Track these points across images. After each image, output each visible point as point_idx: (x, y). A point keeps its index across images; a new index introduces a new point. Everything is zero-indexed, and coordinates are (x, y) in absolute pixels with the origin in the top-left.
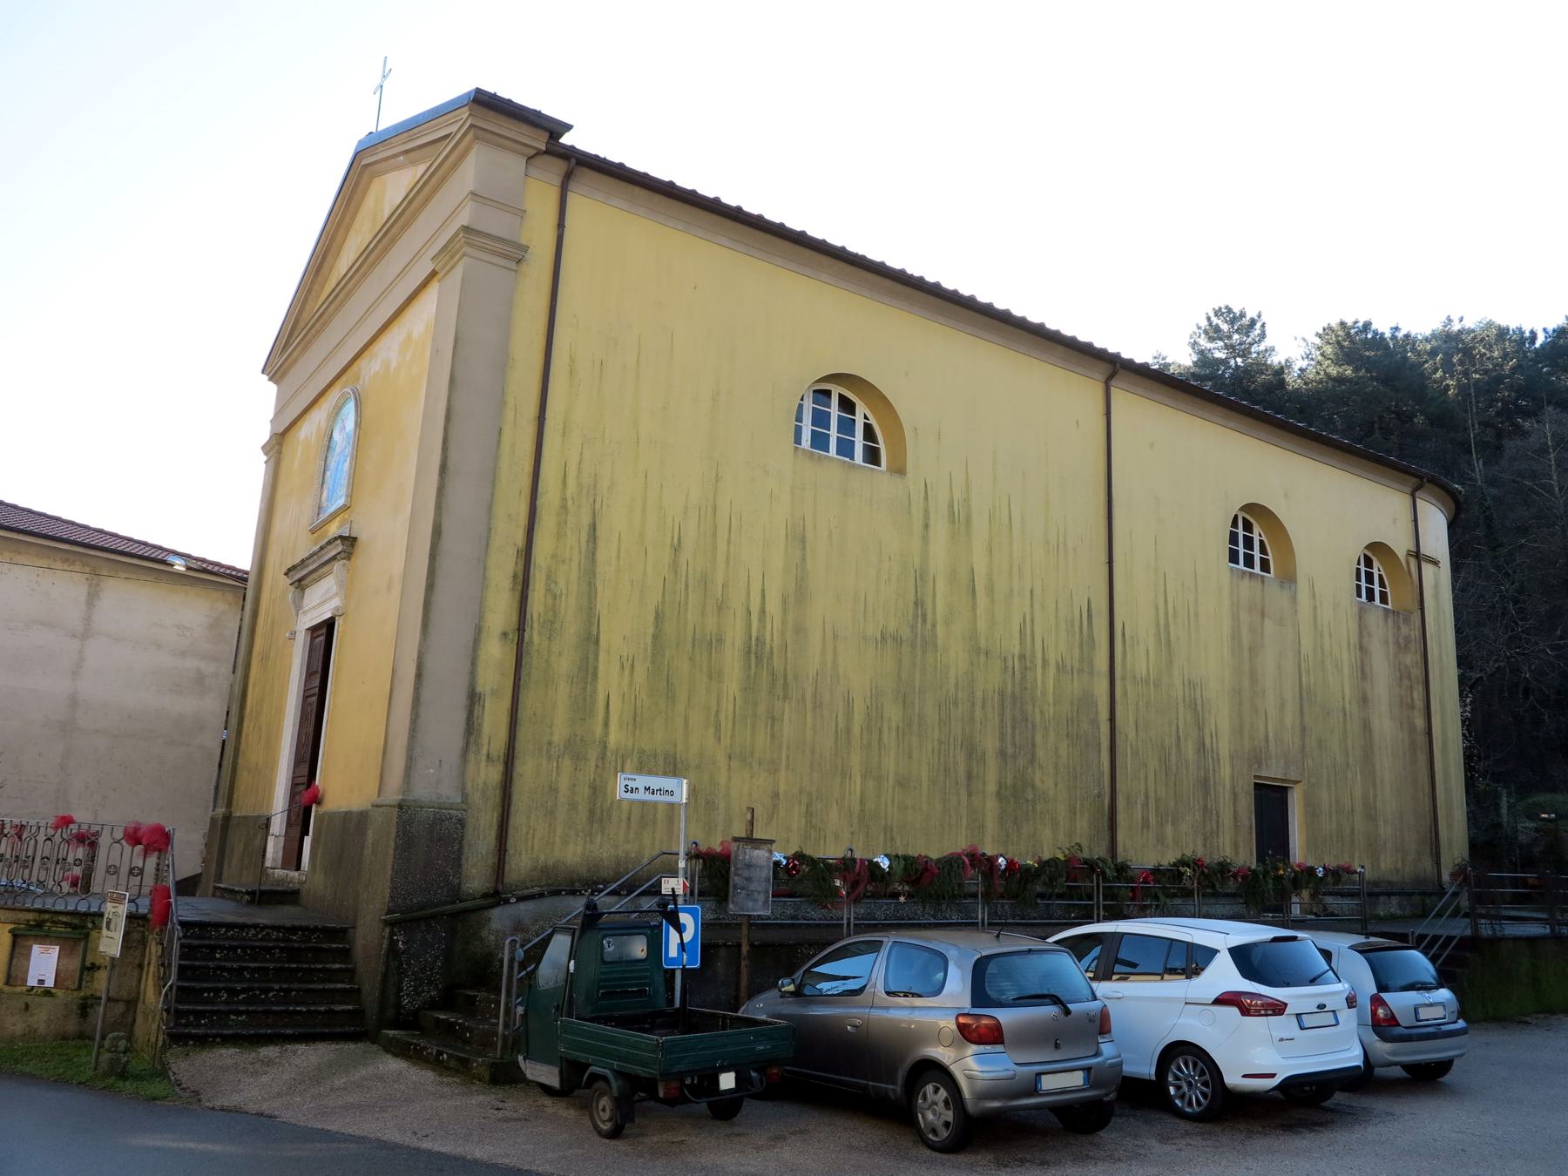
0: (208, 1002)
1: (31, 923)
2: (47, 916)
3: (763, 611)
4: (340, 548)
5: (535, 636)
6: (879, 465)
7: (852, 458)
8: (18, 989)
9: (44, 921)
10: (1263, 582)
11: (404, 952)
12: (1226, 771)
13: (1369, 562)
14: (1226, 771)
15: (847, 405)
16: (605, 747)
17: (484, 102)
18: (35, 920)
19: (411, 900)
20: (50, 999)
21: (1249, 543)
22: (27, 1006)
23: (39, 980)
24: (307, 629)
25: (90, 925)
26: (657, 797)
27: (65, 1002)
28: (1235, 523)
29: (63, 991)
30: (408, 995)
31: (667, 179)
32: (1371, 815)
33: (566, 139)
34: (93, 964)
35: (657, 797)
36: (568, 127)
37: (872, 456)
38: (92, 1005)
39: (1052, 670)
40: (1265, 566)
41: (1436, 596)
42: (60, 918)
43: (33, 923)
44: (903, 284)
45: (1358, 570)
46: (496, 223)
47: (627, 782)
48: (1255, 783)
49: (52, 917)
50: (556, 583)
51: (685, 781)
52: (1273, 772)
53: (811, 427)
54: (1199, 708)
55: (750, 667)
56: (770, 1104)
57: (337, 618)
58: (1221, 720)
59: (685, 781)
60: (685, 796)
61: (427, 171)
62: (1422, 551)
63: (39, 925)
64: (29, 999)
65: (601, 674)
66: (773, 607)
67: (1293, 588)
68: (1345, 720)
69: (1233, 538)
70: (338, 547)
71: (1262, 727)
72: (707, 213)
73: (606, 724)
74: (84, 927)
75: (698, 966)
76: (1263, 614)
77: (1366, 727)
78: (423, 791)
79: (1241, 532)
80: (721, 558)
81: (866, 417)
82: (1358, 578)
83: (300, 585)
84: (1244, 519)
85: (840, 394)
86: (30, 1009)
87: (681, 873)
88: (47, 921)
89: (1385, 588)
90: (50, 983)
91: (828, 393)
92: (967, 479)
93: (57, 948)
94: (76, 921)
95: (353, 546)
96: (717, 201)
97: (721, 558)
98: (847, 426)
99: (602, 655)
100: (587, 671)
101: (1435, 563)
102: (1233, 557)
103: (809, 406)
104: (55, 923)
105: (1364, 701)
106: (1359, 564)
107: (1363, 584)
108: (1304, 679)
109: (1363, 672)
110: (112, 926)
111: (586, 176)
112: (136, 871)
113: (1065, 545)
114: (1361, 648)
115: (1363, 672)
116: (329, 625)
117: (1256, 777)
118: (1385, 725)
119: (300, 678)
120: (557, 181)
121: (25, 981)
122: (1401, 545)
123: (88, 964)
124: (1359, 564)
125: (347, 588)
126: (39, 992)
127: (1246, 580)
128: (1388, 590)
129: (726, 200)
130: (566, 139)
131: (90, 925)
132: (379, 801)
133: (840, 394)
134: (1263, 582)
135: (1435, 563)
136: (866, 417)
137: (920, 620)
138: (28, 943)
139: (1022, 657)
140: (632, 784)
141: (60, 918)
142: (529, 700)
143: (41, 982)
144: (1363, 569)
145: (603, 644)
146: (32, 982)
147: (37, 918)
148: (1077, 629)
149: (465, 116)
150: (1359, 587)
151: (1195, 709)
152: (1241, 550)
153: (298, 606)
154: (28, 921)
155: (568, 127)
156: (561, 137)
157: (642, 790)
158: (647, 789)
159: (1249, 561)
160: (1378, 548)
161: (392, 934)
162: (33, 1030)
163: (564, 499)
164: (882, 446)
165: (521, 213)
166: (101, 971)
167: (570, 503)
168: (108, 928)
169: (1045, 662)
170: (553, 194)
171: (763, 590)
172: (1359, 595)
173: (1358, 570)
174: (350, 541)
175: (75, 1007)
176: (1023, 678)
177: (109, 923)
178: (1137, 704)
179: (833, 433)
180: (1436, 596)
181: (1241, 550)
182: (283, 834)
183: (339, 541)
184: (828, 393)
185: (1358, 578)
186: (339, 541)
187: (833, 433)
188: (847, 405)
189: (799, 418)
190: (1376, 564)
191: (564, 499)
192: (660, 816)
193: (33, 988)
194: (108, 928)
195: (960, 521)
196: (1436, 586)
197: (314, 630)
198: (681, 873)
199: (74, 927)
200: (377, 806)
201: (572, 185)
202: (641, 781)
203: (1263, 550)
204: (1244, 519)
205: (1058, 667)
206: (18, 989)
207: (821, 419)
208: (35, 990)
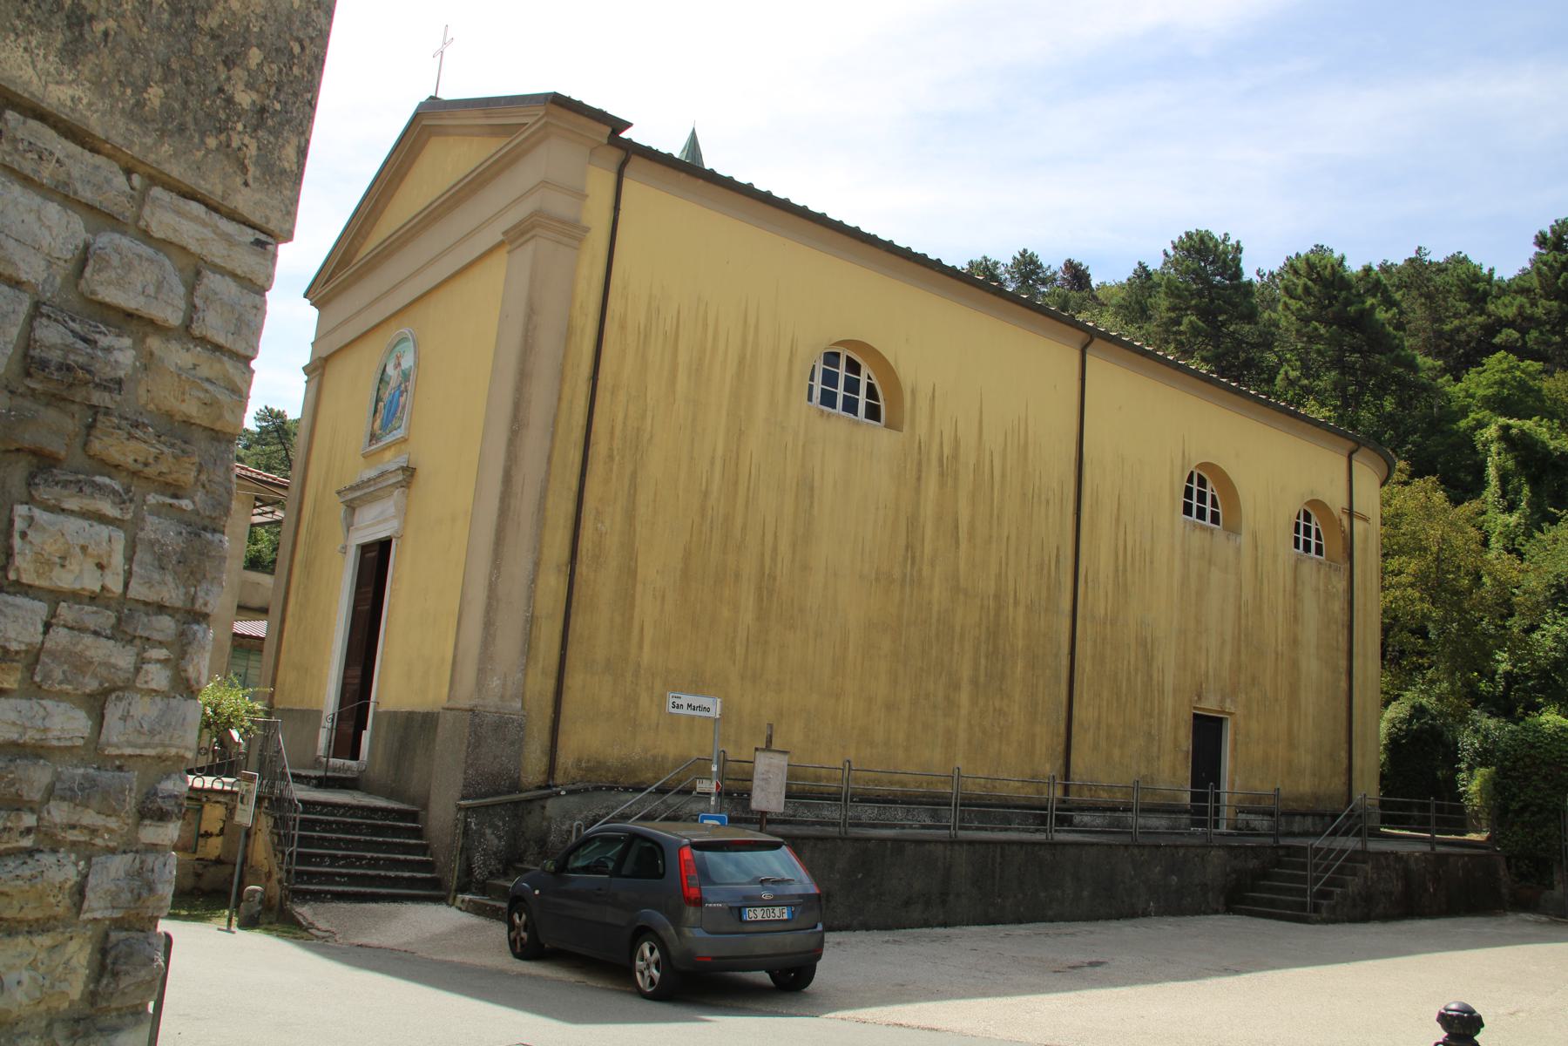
0: (315, 865)
3: (775, 549)
4: (400, 478)
5: (583, 569)
6: (879, 420)
7: (856, 414)
10: (1212, 533)
11: (476, 832)
12: (1169, 702)
13: (1307, 517)
14: (1169, 702)
15: (853, 366)
16: (639, 666)
17: (559, 102)
19: (480, 789)
21: (1307, 531)
24: (358, 545)
25: (204, 799)
26: (697, 713)
28: (1190, 480)
30: (479, 868)
31: (801, 205)
32: (1292, 745)
33: (625, 135)
34: (206, 832)
35: (697, 713)
36: (628, 125)
37: (873, 413)
39: (1021, 610)
40: (1319, 551)
41: (1365, 550)
45: (1297, 525)
46: (559, 205)
47: (674, 700)
48: (1194, 714)
50: (602, 522)
51: (719, 700)
52: (1210, 705)
53: (821, 386)
54: (1149, 646)
55: (762, 600)
56: (533, 963)
57: (394, 540)
58: (1167, 658)
59: (719, 700)
60: (718, 712)
61: (497, 152)
62: (1355, 509)
65: (638, 602)
66: (784, 547)
67: (1238, 540)
68: (1277, 659)
69: (1188, 493)
71: (1203, 665)
72: (965, 286)
73: (641, 647)
74: (199, 800)
76: (1210, 562)
77: (1295, 665)
78: (491, 701)
79: (1195, 487)
80: (741, 501)
81: (869, 378)
82: (1297, 531)
83: (351, 507)
84: (1199, 475)
85: (848, 357)
87: (714, 775)
89: (1217, 508)
91: (837, 355)
92: (956, 436)
95: (412, 475)
96: (805, 208)
97: (741, 501)
98: (852, 386)
99: (639, 587)
100: (626, 600)
101: (1365, 519)
102: (1187, 510)
103: (820, 367)
105: (1295, 642)
106: (1298, 518)
107: (1301, 537)
108: (1243, 622)
109: (1295, 617)
110: (245, 801)
111: (636, 162)
112: (203, 751)
113: (1040, 497)
114: (1295, 595)
115: (1295, 617)
116: (384, 546)
117: (1195, 708)
118: (1311, 666)
120: (615, 168)
122: (1337, 501)
123: (202, 832)
124: (1298, 518)
125: (404, 513)
127: (1197, 532)
128: (1220, 511)
129: (719, 171)
130: (625, 135)
131: (204, 799)
132: (451, 704)
133: (848, 357)
134: (1212, 533)
135: (1365, 519)
136: (869, 378)
137: (909, 562)
139: (997, 597)
140: (678, 702)
142: (577, 622)
144: (1302, 522)
145: (639, 577)
148: (1045, 572)
149: (541, 113)
150: (1297, 540)
151: (1146, 646)
152: (1195, 503)
153: (349, 526)
155: (628, 125)
156: (622, 131)
157: (685, 706)
158: (689, 706)
159: (1307, 548)
160: (1316, 504)
161: (466, 817)
163: (611, 449)
164: (882, 404)
165: (581, 195)
167: (615, 452)
168: (242, 802)
169: (1016, 603)
170: (611, 178)
171: (776, 533)
172: (1297, 546)
173: (1297, 525)
174: (409, 472)
176: (997, 615)
177: (242, 798)
178: (1095, 642)
179: (840, 392)
180: (1365, 550)
181: (1195, 503)
184: (837, 355)
185: (1297, 531)
186: (400, 472)
187: (840, 392)
188: (853, 366)
189: (812, 379)
190: (1314, 519)
191: (611, 449)
194: (242, 802)
195: (948, 471)
196: (1366, 539)
197: (365, 548)
198: (714, 775)
200: (448, 709)
201: (1088, 351)
202: (685, 699)
203: (1214, 504)
204: (1199, 475)
205: (1027, 606)
207: (830, 379)
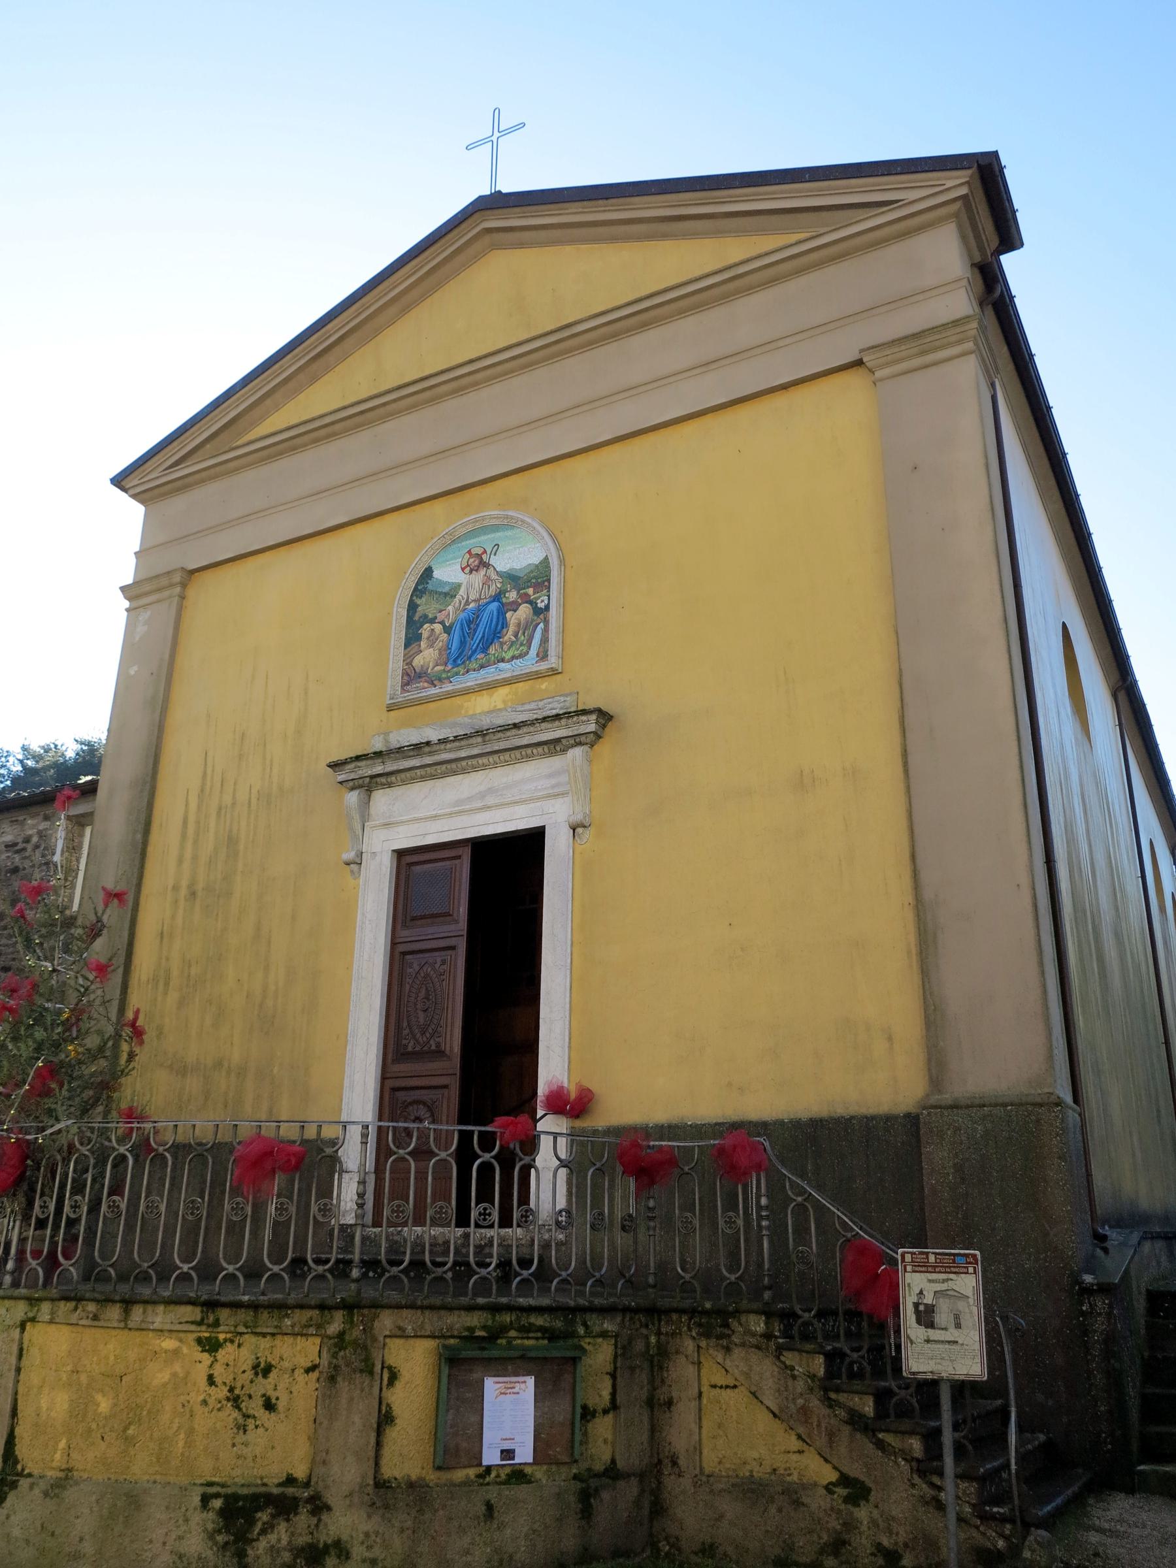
1: (479, 1333)
2: (507, 1318)
8: (460, 1475)
9: (503, 1329)
18: (484, 1328)
20: (524, 1487)
22: (489, 1507)
23: (502, 1451)
27: (557, 1490)
29: (545, 1467)
38: (596, 1490)
42: (532, 1319)
43: (482, 1333)
44: (651, 431)
49: (518, 1318)
63: (494, 1335)
64: (492, 1493)
70: (590, 725)
74: (573, 1335)
75: (985, 1378)
86: (496, 1514)
88: (511, 1326)
90: (525, 1454)
93: (531, 1381)
94: (559, 1324)
104: (526, 1330)
119: (390, 882)
121: (476, 1457)
126: (503, 1477)
138: (475, 1376)
141: (532, 1319)
143: (508, 1454)
146: (490, 1457)
147: (490, 1323)
154: (471, 1329)
162: (505, 1556)
166: (597, 1420)
175: (572, 1499)
182: (373, 1170)
183: (594, 717)
186: (594, 717)
192: (444, 1136)
193: (489, 1469)
199: (552, 1335)
206: (460, 1475)
208: (493, 1474)
